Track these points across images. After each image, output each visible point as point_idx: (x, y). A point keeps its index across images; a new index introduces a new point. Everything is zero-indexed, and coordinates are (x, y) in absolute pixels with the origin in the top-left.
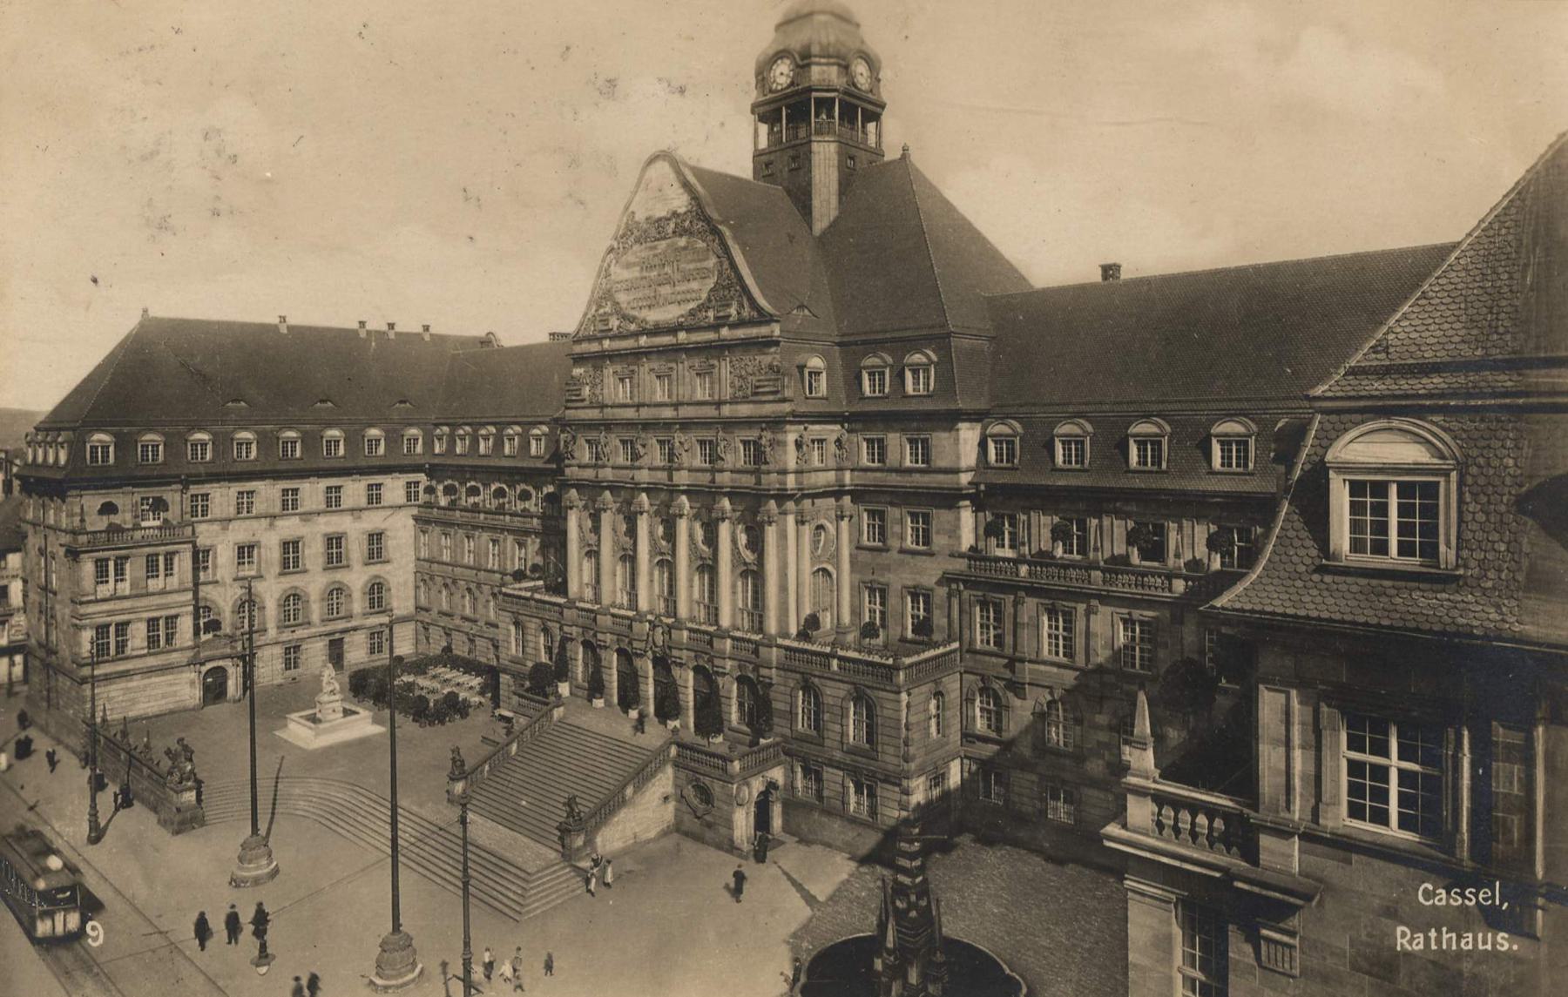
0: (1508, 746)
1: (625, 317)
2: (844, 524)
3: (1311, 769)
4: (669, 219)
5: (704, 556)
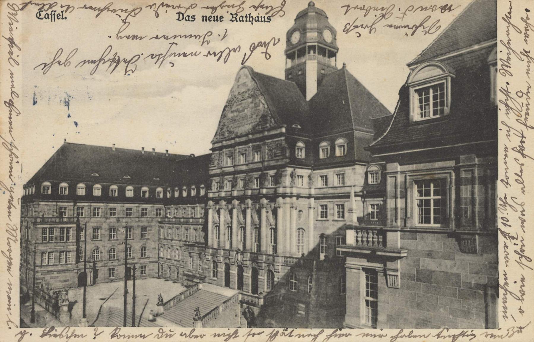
0: (466, 178)
1: (230, 132)
2: (312, 211)
3: (404, 206)
4: (246, 92)
5: (256, 223)
